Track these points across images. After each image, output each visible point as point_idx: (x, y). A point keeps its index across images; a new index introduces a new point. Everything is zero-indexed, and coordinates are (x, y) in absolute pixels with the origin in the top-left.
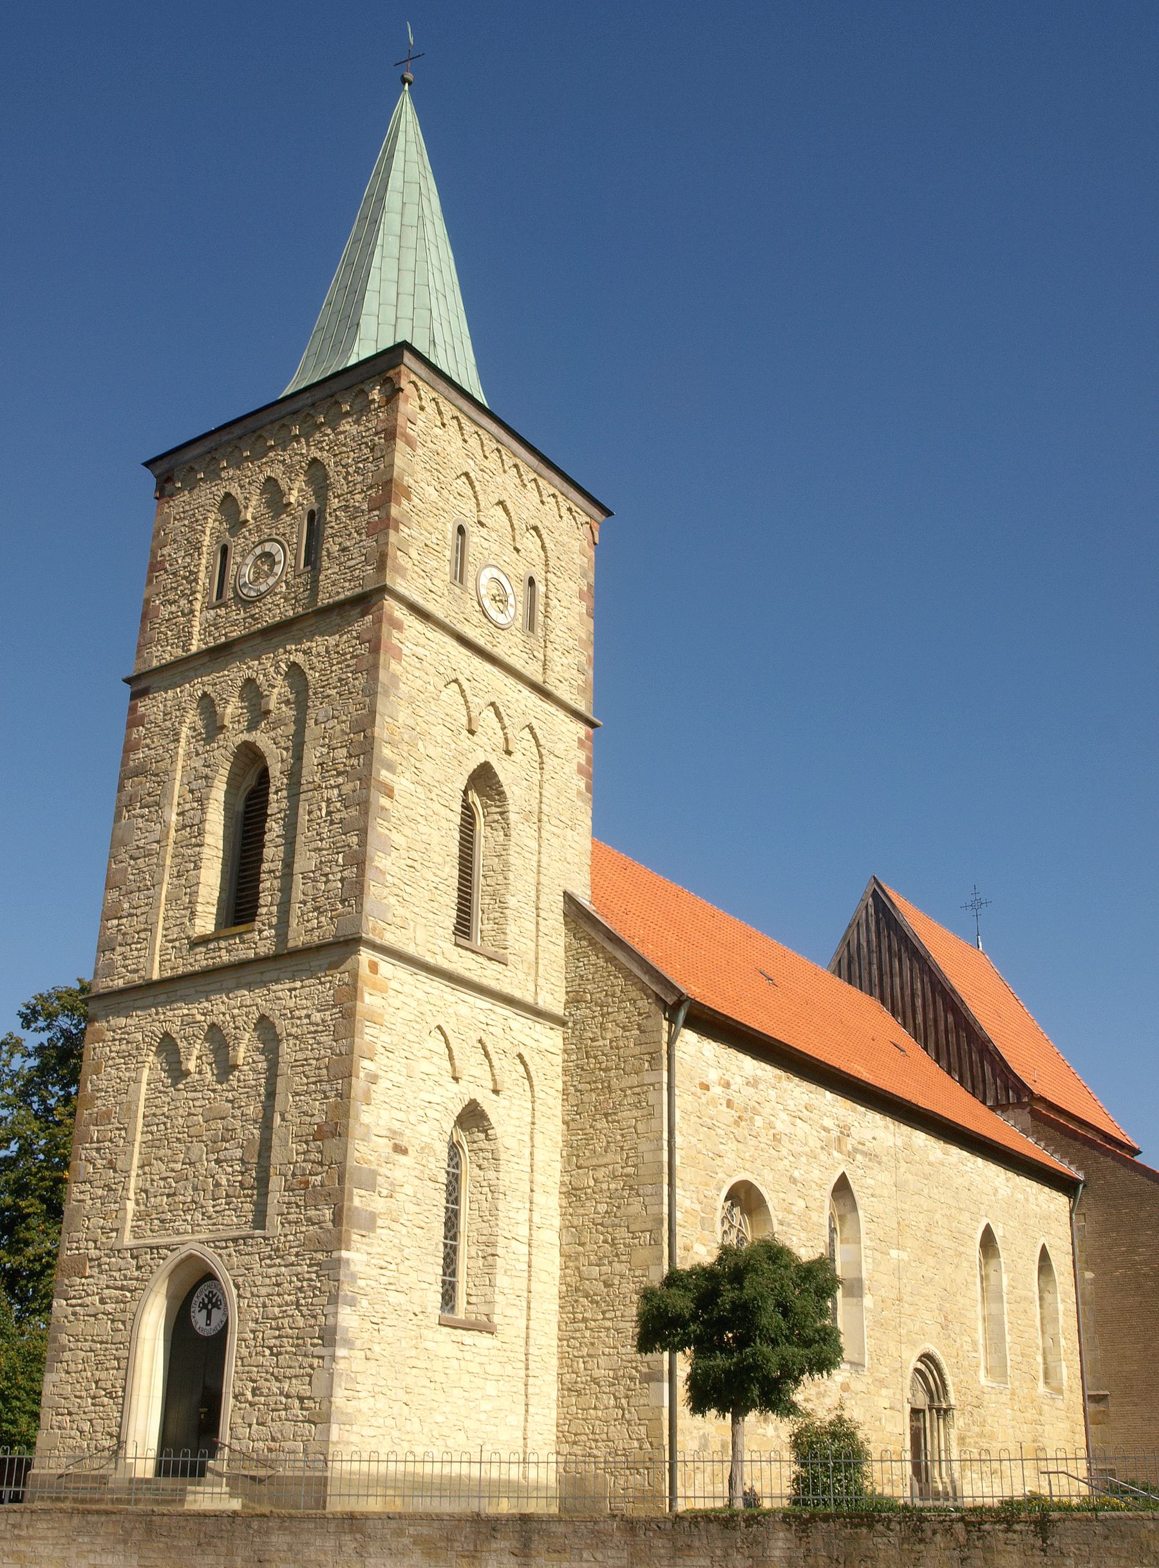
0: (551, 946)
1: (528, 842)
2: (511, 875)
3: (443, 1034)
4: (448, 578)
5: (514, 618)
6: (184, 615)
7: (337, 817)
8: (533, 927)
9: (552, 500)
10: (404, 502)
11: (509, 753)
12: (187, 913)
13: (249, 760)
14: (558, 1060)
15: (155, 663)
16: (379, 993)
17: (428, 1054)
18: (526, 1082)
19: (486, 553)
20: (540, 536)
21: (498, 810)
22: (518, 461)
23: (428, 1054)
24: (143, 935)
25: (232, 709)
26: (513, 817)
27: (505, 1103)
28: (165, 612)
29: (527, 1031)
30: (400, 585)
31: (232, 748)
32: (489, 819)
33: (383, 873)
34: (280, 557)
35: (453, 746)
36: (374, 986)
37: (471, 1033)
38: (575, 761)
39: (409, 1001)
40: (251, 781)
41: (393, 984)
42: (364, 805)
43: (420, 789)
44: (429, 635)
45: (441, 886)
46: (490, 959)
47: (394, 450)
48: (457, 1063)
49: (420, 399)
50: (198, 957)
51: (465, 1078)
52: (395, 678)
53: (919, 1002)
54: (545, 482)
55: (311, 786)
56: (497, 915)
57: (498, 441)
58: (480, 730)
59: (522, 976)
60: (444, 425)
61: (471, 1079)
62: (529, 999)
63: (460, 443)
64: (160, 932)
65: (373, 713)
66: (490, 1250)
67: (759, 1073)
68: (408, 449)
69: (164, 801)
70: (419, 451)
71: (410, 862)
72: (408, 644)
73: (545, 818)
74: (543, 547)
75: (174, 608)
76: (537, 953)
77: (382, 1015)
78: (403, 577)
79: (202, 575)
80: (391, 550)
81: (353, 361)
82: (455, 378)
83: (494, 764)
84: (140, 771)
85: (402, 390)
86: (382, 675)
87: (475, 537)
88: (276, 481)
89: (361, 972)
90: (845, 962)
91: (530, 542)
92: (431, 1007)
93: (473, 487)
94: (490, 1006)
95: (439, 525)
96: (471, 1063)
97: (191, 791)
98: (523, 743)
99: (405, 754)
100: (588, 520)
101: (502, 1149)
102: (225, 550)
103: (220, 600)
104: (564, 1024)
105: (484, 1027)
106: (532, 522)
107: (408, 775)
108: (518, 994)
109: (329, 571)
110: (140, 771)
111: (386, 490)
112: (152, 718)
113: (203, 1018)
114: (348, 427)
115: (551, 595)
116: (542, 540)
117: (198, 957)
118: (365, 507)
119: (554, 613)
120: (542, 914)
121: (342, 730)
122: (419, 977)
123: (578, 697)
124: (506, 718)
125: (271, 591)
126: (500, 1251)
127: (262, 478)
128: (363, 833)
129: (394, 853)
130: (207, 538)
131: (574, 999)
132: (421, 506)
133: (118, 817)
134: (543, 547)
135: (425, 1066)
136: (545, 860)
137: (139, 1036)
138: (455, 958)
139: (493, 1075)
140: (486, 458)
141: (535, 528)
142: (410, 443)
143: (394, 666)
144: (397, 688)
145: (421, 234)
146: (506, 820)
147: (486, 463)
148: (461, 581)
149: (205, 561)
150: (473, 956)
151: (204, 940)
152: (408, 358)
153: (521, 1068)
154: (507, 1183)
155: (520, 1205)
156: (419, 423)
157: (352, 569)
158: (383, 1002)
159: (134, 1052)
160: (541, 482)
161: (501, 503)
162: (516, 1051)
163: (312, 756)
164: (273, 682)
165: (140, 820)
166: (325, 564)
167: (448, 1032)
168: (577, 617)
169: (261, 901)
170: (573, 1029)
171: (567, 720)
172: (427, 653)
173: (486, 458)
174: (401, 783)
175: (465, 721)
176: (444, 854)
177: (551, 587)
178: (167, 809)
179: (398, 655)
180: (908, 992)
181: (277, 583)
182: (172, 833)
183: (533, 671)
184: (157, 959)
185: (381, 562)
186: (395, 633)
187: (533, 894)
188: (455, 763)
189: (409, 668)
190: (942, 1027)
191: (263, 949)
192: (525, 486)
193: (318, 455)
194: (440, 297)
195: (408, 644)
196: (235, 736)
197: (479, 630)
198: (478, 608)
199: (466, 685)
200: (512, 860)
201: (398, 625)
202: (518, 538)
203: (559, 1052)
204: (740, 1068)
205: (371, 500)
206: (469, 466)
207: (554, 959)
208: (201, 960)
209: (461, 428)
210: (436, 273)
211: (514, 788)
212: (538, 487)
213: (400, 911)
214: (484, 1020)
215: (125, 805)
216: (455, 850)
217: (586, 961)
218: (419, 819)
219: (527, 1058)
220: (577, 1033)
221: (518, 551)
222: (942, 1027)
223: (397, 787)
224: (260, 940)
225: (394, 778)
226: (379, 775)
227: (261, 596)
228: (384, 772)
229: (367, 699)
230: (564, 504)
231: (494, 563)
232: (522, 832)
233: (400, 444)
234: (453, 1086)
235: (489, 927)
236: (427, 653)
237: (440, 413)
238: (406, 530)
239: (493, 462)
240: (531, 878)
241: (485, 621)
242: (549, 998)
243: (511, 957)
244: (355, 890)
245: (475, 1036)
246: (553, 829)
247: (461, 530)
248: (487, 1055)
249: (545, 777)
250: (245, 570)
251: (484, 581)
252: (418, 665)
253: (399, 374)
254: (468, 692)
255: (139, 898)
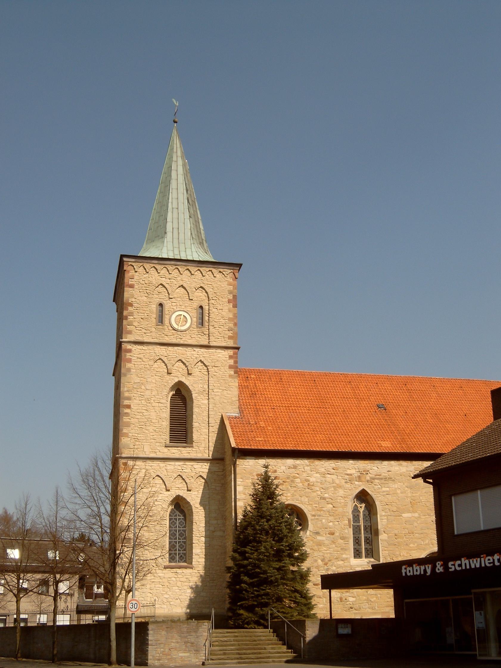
44: (144, 348)
152: (125, 259)
189: (136, 363)
190: (223, 657)
201: (130, 351)
214: (180, 468)
222: (223, 657)
225: (131, 401)
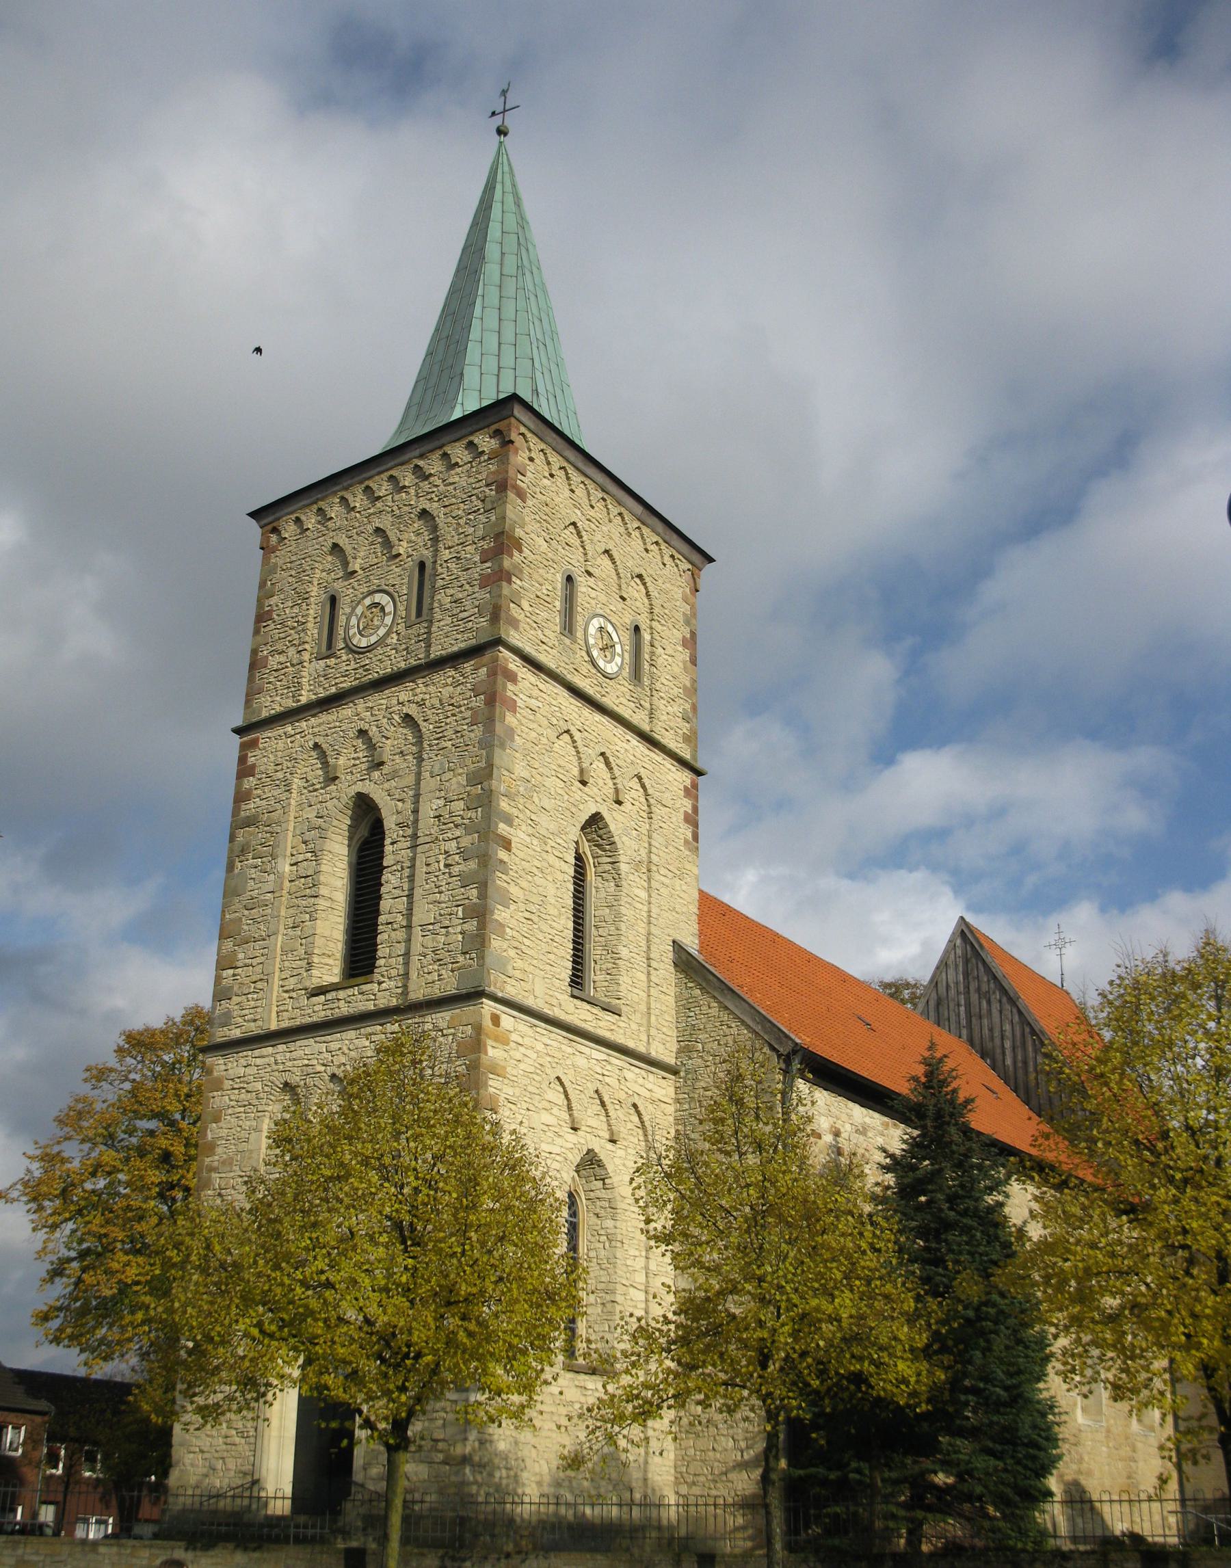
0: (662, 996)
1: (637, 891)
2: (623, 926)
3: (562, 1084)
4: (558, 629)
5: (621, 668)
6: (293, 665)
7: (456, 870)
8: (644, 977)
9: (654, 547)
10: (516, 553)
11: (619, 803)
12: (304, 963)
13: (365, 809)
14: (670, 1109)
15: (265, 714)
16: (500, 1046)
17: (547, 1105)
18: (640, 1132)
19: (593, 602)
20: (644, 584)
21: (609, 860)
22: (623, 510)
23: (547, 1105)
24: (259, 985)
25: (347, 758)
26: (624, 868)
27: (621, 1153)
28: (273, 662)
29: (641, 1081)
30: (514, 638)
31: (345, 799)
32: (600, 869)
33: (502, 926)
34: (389, 608)
35: (566, 797)
36: (496, 1039)
37: (589, 1084)
38: (682, 810)
39: (529, 1052)
40: (364, 832)
41: (514, 1037)
42: (485, 860)
43: (535, 842)
44: (541, 686)
45: (557, 938)
46: (604, 1009)
47: (505, 502)
48: (575, 1113)
49: (530, 450)
50: (316, 1008)
51: (583, 1128)
52: (511, 732)
53: (1008, 1044)
54: (648, 530)
55: (428, 839)
56: (610, 965)
57: (603, 490)
58: (591, 781)
59: (634, 1026)
60: (552, 476)
61: (589, 1130)
62: (642, 1049)
63: (567, 493)
64: (277, 983)
65: (490, 766)
66: (608, 1298)
67: (867, 1120)
68: (519, 501)
69: (279, 851)
70: (530, 502)
71: (527, 915)
72: (521, 696)
73: (654, 868)
74: (648, 595)
75: (282, 658)
76: (649, 1003)
77: (505, 1068)
78: (516, 628)
79: (310, 625)
80: (503, 602)
81: (457, 414)
82: (567, 432)
83: (605, 814)
84: (251, 822)
85: (512, 442)
86: (498, 728)
87: (583, 585)
88: (384, 532)
89: (484, 1024)
90: (932, 1004)
91: (635, 591)
92: (549, 1059)
93: (581, 537)
94: (604, 1057)
95: (549, 576)
96: (590, 1116)
97: (305, 842)
98: (633, 793)
99: (521, 807)
100: (690, 567)
101: (619, 1198)
102: (333, 600)
103: (329, 650)
104: (675, 1072)
105: (600, 1077)
106: (637, 571)
107: (524, 828)
108: (631, 1044)
109: (442, 622)
110: (251, 822)
111: (502, 543)
112: (262, 768)
113: (323, 1068)
114: (457, 479)
115: (656, 643)
116: (646, 588)
117: (316, 1008)
118: (477, 558)
119: (660, 661)
120: (654, 964)
121: (458, 783)
122: (538, 1029)
123: (683, 745)
124: (615, 768)
125: (381, 642)
126: (619, 1298)
127: (370, 529)
128: (483, 887)
129: (513, 907)
130: (315, 589)
131: (685, 1050)
132: (531, 557)
133: (230, 867)
134: (648, 595)
135: (546, 1118)
136: (655, 911)
137: (259, 1086)
138: (571, 1009)
139: (609, 1125)
140: (592, 507)
141: (640, 576)
142: (521, 495)
143: (510, 719)
144: (513, 740)
145: (520, 284)
146: (617, 870)
147: (592, 512)
148: (571, 631)
149: (314, 610)
150: (588, 1007)
151: (321, 991)
152: (518, 411)
153: (636, 1119)
154: (624, 1232)
155: (637, 1253)
156: (529, 474)
157: (466, 620)
158: (506, 1055)
159: (255, 1102)
160: (645, 530)
161: (607, 552)
162: (631, 1101)
163: (429, 807)
164: (386, 733)
165: (253, 870)
166: (437, 616)
167: (567, 1084)
168: (681, 665)
169: (379, 953)
170: (684, 1078)
171: (674, 769)
172: (540, 705)
173: (592, 507)
174: (519, 835)
175: (576, 772)
176: (559, 906)
177: (656, 636)
178: (279, 860)
179: (513, 707)
180: (997, 1034)
181: (388, 634)
182: (287, 884)
183: (640, 719)
184: (275, 1009)
185: (496, 614)
186: (510, 686)
187: (643, 943)
188: (568, 814)
189: (524, 721)
191: (383, 1001)
192: (629, 534)
193: (427, 506)
194: (541, 346)
195: (521, 696)
196: (347, 788)
197: (588, 681)
198: (587, 658)
199: (577, 736)
200: (623, 910)
201: (512, 678)
202: (624, 586)
203: (670, 1101)
204: (850, 1116)
205: (484, 552)
206: (576, 516)
207: (664, 1008)
208: (318, 1010)
209: (568, 478)
210: (537, 322)
211: (624, 838)
212: (642, 535)
213: (519, 964)
215: (237, 852)
216: (570, 902)
217: (697, 1010)
218: (535, 870)
219: (641, 1108)
220: (689, 1082)
221: (623, 599)
223: (514, 840)
224: (381, 991)
225: (512, 831)
226: (497, 828)
227: (370, 648)
228: (502, 825)
229: (484, 752)
230: (667, 551)
231: (601, 612)
232: (634, 885)
233: (511, 495)
234: (572, 1138)
235: (601, 977)
236: (540, 705)
237: (549, 463)
238: (518, 582)
239: (598, 512)
240: (642, 928)
241: (594, 671)
242: (661, 1048)
243: (624, 1009)
244: (477, 943)
245: (591, 1087)
246: (663, 879)
247: (569, 579)
248: (603, 1104)
249: (654, 826)
250: (350, 621)
251: (592, 630)
252: (532, 717)
253: (509, 425)
254: (579, 743)
255: (254, 949)
